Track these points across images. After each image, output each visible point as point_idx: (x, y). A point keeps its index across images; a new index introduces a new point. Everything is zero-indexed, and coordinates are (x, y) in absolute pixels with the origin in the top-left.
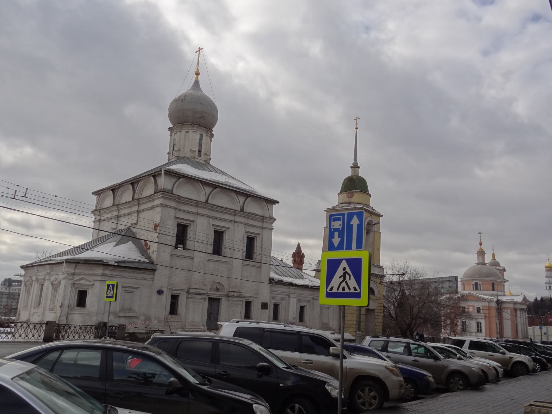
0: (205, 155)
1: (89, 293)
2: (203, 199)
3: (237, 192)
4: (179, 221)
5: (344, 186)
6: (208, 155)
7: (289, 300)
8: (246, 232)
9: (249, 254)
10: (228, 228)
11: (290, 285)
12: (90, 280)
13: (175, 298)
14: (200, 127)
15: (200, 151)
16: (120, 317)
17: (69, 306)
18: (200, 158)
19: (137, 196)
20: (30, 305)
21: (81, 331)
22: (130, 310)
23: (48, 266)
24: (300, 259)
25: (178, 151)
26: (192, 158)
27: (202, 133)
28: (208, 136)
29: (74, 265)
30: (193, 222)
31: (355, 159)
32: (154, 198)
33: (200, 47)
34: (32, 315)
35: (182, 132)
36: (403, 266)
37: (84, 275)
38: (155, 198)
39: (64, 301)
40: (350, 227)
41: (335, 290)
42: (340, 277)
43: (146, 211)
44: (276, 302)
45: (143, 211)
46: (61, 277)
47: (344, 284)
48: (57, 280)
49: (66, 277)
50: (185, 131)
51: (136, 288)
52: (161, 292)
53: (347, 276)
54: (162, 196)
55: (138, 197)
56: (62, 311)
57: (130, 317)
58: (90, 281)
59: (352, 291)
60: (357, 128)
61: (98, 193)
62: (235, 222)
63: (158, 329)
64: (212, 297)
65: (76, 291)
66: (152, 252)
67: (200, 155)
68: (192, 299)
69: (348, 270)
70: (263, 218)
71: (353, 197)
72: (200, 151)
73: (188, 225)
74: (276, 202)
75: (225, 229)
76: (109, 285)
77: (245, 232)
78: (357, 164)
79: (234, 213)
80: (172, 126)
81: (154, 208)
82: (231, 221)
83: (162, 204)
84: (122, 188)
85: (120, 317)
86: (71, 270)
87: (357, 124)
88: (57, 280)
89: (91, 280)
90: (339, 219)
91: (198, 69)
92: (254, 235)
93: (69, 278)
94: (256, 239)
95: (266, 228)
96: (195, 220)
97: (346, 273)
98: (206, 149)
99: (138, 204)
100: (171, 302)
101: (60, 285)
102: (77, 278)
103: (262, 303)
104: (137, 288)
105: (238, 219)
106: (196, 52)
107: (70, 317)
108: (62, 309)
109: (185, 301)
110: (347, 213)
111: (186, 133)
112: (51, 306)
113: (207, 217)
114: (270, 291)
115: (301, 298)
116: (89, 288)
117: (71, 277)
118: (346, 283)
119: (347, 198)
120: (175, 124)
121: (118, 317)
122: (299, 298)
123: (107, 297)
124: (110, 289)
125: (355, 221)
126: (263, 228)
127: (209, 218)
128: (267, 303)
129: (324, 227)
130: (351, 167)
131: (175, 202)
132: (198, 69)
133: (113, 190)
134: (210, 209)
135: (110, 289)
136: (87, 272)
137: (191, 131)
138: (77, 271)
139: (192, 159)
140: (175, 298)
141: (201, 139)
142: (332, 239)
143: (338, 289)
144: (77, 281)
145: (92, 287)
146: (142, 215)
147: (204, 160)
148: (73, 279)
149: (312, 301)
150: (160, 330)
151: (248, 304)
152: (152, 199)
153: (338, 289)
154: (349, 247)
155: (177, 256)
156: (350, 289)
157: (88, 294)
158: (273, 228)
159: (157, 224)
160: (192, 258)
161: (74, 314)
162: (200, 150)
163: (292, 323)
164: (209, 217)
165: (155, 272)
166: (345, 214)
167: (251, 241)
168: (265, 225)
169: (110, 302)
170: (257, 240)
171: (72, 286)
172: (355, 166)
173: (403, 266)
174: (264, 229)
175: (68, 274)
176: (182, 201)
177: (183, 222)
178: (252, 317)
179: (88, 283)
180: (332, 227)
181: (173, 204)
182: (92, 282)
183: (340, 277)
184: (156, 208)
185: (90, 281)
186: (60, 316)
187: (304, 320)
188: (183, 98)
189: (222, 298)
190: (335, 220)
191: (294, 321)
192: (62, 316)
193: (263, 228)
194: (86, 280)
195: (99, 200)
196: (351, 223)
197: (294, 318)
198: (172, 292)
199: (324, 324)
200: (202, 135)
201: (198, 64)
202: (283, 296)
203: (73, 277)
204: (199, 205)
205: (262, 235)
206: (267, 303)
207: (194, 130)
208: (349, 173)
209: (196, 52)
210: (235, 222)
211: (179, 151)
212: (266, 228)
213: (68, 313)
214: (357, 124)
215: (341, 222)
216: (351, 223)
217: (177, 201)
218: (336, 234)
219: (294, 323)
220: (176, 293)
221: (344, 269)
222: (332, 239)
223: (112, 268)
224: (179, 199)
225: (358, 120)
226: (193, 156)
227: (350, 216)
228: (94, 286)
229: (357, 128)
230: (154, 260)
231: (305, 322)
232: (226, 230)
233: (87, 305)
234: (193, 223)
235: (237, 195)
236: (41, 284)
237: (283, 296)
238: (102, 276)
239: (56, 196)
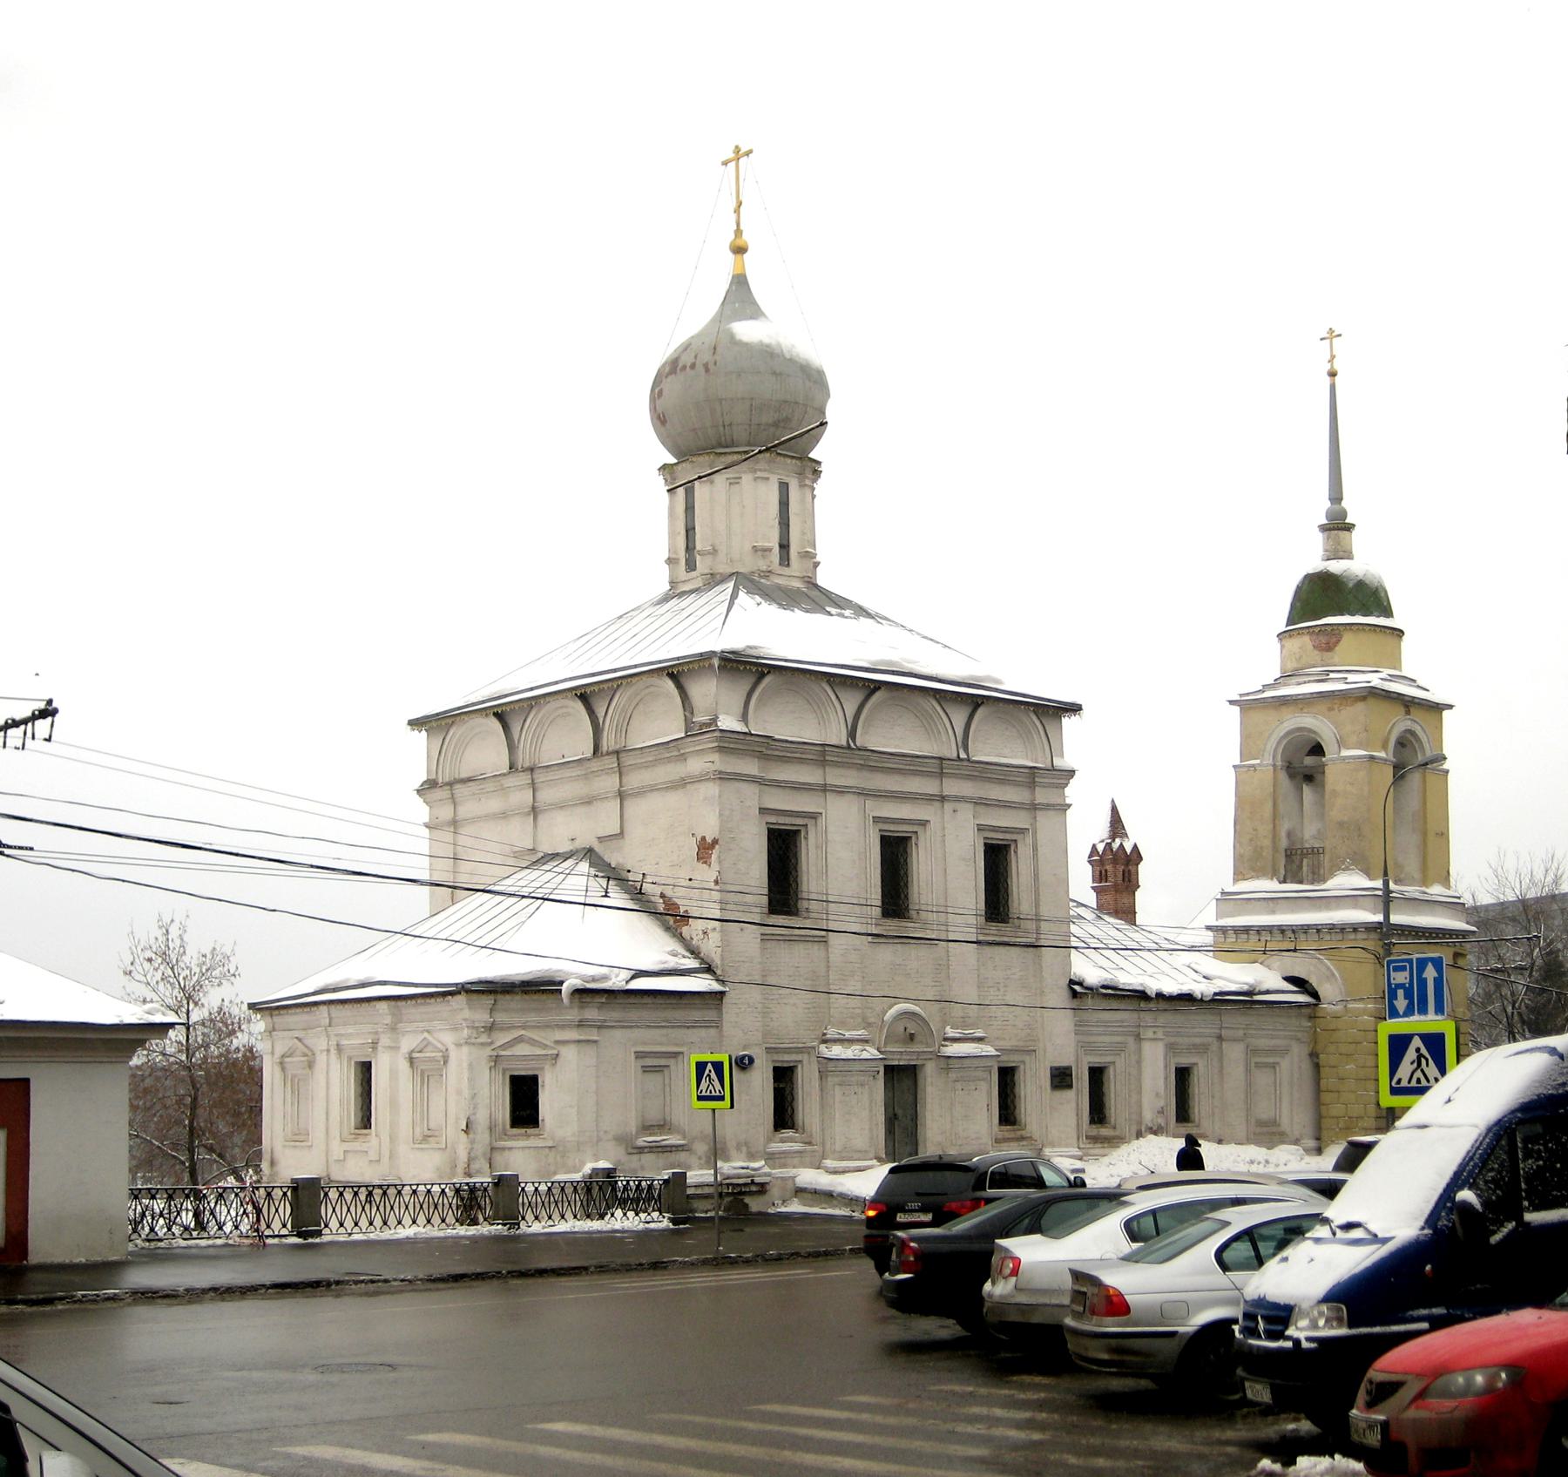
0: (805, 556)
1: (546, 1082)
2: (837, 735)
3: (942, 695)
4: (773, 819)
5: (1298, 604)
6: (809, 557)
7: (1140, 1050)
8: (981, 828)
9: (997, 903)
10: (924, 823)
11: (1138, 997)
12: (545, 1042)
13: (784, 1077)
14: (779, 458)
15: (784, 547)
16: (641, 1150)
17: (493, 1126)
18: (786, 571)
19: (608, 742)
20: (322, 1126)
21: (446, 1201)
22: (663, 1126)
23: (383, 1005)
24: (1124, 871)
25: (709, 553)
26: (760, 576)
27: (786, 479)
28: (806, 485)
29: (488, 1001)
30: (814, 816)
31: (1336, 496)
32: (682, 751)
33: (737, 147)
34: (338, 1161)
35: (716, 481)
36: (1539, 875)
37: (524, 1027)
38: (687, 751)
39: (474, 1114)
40: (1423, 983)
41: (1404, 1083)
42: (1412, 1063)
43: (655, 794)
44: (1097, 1060)
45: (641, 792)
46: (448, 1039)
47: (1418, 1074)
48: (425, 1046)
49: (470, 1038)
50: (727, 479)
51: (674, 1055)
52: (747, 1062)
53: (1423, 1061)
54: (716, 744)
55: (616, 743)
56: (472, 1142)
57: (669, 1149)
58: (545, 1046)
59: (718, 1094)
60: (1333, 374)
61: (434, 724)
62: (943, 799)
63: (752, 1180)
64: (896, 1063)
65: (504, 1079)
66: (701, 933)
67: (785, 559)
68: (837, 1076)
69: (1424, 1051)
70: (1031, 776)
71: (1337, 648)
72: (784, 547)
73: (799, 831)
74: (1075, 709)
75: (915, 828)
76: (701, 1067)
77: (978, 830)
78: (1344, 514)
79: (940, 767)
80: (673, 460)
81: (688, 786)
82: (929, 799)
83: (720, 773)
84: (539, 711)
85: (641, 1150)
86: (482, 1017)
87: (1333, 357)
88: (425, 1046)
89: (548, 1043)
90: (1403, 969)
91: (738, 232)
92: (1008, 836)
93: (479, 1040)
94: (1012, 848)
95: (1048, 807)
96: (820, 811)
97: (1420, 1056)
98: (804, 534)
99: (617, 769)
100: (775, 1088)
101: (445, 1062)
102: (502, 1038)
103: (1051, 1068)
104: (675, 1055)
105: (952, 787)
106: (725, 163)
107: (499, 1158)
108: (471, 1136)
109: (816, 1083)
110: (1417, 959)
111: (730, 484)
112: (418, 1130)
113: (856, 796)
114: (1076, 1025)
115: (1180, 1040)
116: (542, 1069)
117: (484, 1039)
118: (1422, 1071)
119: (1316, 652)
120: (684, 453)
121: (635, 1151)
122: (1172, 1040)
123: (700, 1098)
124: (709, 1075)
125: (1430, 973)
126: (1035, 809)
127: (862, 798)
128: (1069, 1068)
129: (1234, 767)
130: (1323, 528)
131: (756, 759)
132: (738, 232)
133: (501, 715)
134: (862, 767)
135: (709, 1075)
136: (533, 1018)
137: (747, 479)
138: (501, 1017)
139: (762, 581)
140: (784, 1077)
141: (784, 504)
142: (1394, 1002)
143: (1409, 1082)
144: (504, 1050)
145: (553, 1065)
146: (635, 808)
147: (803, 577)
148: (492, 1043)
149: (1215, 1045)
150: (756, 1181)
151: (1007, 1077)
152: (676, 753)
153: (1409, 1082)
154: (1423, 1010)
155: (778, 938)
156: (1428, 1081)
157: (543, 1086)
158: (1068, 801)
159: (709, 840)
160: (822, 939)
161: (510, 1149)
162: (785, 543)
163: (1155, 1128)
164: (864, 793)
165: (722, 1000)
166: (1412, 959)
167: (997, 858)
168: (1041, 796)
169: (714, 1110)
170: (1016, 852)
171: (493, 1064)
172: (1337, 525)
173: (1539, 875)
174: (1037, 812)
175: (473, 1027)
176: (777, 753)
177: (785, 822)
178: (1023, 1121)
179: (539, 1052)
180: (1392, 981)
181: (751, 767)
182: (552, 1048)
183: (1412, 1063)
184: (696, 786)
185: (545, 1046)
186: (469, 1160)
187: (1192, 1116)
188: (706, 357)
189: (924, 1065)
190: (1396, 969)
191: (1161, 1121)
192: (474, 1159)
193: (1034, 807)
194: (533, 1042)
195: (445, 747)
196: (1424, 976)
197: (1159, 1112)
198: (776, 1057)
199: (1260, 1123)
200: (787, 484)
201: (737, 211)
202: (1119, 1039)
203: (489, 1036)
204: (827, 758)
205: (1035, 833)
206: (1069, 1068)
207: (759, 474)
208: (1311, 558)
209: (725, 163)
210: (943, 799)
211: (714, 552)
212: (1048, 807)
213: (492, 1149)
214: (1333, 357)
215: (1406, 974)
216: (1424, 976)
217: (763, 757)
218: (1400, 993)
219: (1162, 1128)
220: (786, 1059)
221: (1418, 1050)
222: (1394, 1002)
223: (604, 1000)
224: (766, 749)
225: (1334, 340)
226: (764, 568)
227: (1422, 963)
228: (560, 1061)
229: (1333, 374)
230: (713, 961)
231: (1197, 1119)
232: (916, 832)
233: (543, 1120)
234: (814, 821)
235: (942, 703)
236: (353, 1063)
237: (1119, 1039)
238: (579, 1026)
239: (690, 880)
